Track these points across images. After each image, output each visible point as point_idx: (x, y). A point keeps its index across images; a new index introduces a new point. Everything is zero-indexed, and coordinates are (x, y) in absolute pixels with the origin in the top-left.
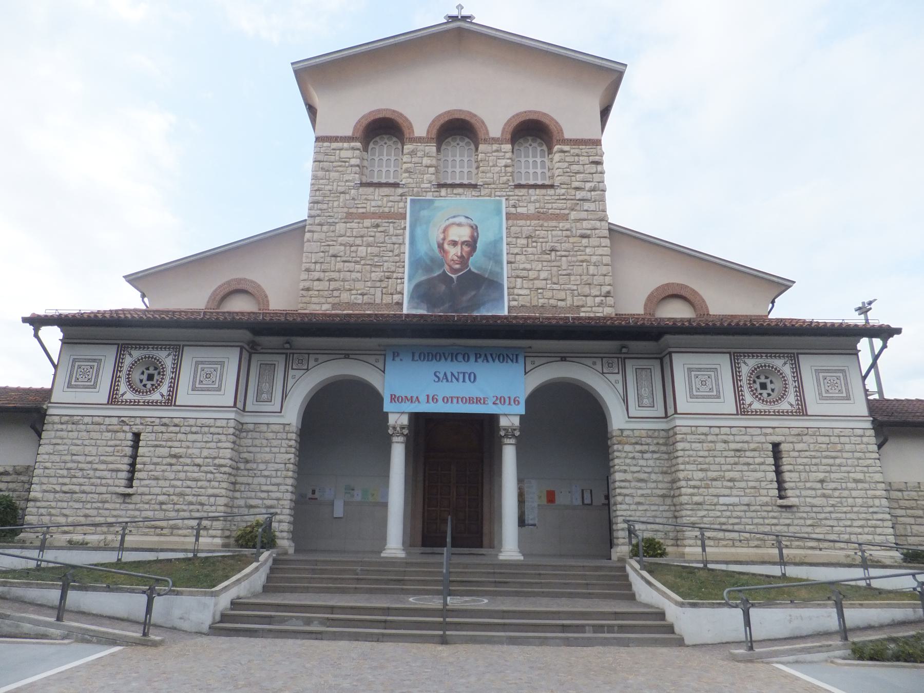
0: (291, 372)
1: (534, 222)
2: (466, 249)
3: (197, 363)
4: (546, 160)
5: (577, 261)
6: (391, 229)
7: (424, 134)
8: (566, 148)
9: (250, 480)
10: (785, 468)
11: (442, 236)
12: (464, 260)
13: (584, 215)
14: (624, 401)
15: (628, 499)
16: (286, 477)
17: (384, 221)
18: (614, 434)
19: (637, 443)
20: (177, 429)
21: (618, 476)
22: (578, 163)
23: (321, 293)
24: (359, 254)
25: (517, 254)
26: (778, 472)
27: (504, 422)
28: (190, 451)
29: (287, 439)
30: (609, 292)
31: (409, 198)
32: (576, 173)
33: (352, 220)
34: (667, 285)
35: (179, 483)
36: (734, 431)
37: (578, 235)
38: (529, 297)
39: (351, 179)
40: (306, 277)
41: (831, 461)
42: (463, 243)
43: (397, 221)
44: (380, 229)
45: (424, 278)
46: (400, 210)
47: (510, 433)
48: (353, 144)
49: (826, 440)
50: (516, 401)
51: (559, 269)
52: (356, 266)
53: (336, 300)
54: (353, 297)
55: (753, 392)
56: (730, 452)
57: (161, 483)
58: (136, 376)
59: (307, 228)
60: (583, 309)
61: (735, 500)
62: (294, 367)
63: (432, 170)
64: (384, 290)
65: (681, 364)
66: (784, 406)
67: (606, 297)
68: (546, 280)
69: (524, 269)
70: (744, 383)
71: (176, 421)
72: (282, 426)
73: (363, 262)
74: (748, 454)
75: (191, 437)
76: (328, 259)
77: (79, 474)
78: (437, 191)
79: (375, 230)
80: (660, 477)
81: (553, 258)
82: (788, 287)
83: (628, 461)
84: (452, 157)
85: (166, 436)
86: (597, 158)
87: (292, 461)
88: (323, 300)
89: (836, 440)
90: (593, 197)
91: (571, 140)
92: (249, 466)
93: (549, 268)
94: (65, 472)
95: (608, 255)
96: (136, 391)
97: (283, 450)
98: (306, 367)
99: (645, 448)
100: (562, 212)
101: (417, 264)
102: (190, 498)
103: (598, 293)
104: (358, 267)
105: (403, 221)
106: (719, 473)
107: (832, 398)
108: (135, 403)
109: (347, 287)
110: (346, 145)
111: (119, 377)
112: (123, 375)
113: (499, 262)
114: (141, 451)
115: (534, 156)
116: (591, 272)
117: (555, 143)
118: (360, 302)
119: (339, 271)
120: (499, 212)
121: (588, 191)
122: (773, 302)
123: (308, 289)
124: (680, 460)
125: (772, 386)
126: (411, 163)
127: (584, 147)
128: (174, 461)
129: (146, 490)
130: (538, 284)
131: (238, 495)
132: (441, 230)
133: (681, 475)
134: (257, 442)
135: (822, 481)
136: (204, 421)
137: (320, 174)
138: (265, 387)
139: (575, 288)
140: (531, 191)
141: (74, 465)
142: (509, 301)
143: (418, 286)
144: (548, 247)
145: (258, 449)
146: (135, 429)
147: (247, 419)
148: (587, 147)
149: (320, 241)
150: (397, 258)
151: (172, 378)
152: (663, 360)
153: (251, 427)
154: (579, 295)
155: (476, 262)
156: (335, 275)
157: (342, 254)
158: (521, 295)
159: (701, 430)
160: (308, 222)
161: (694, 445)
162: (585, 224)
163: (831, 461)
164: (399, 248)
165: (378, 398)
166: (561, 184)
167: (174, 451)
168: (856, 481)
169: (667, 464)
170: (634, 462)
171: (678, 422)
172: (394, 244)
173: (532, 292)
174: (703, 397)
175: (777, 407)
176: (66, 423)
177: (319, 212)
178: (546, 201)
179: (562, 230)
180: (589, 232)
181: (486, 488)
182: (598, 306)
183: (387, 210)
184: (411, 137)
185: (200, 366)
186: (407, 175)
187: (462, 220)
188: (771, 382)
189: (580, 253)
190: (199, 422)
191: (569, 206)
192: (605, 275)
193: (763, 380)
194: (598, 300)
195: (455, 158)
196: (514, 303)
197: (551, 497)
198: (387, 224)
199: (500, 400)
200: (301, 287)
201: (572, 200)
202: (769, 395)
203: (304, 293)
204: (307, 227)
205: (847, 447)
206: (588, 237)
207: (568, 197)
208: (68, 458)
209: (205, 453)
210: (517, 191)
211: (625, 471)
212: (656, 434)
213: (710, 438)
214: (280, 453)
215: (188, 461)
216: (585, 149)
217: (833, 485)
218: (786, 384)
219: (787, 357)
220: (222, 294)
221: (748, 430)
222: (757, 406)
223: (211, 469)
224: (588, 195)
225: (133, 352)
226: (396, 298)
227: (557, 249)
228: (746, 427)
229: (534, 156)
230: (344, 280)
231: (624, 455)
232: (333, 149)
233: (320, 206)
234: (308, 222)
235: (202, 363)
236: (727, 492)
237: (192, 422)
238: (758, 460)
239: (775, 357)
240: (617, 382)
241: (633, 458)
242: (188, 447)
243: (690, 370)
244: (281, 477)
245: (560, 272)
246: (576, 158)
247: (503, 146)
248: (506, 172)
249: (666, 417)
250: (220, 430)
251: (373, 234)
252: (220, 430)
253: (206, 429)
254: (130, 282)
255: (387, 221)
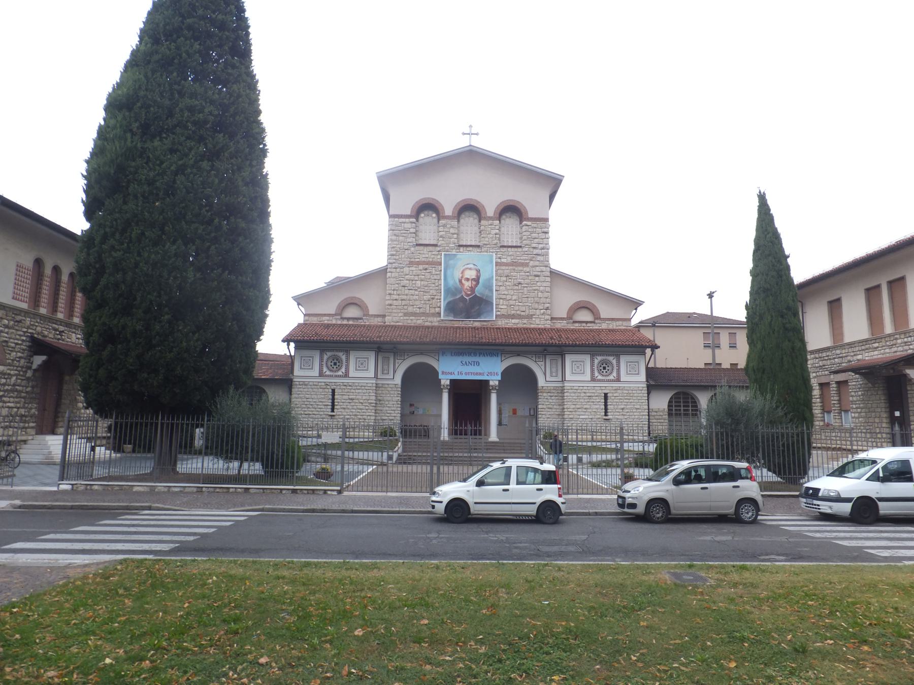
0: (397, 361)
1: (511, 268)
2: (474, 283)
6: (434, 271)
9: (382, 408)
10: (608, 404)
11: (461, 275)
12: (472, 289)
13: (537, 263)
15: (544, 416)
16: (397, 407)
21: (540, 406)
22: (535, 232)
23: (398, 307)
26: (606, 405)
27: (491, 383)
28: (358, 397)
30: (548, 307)
31: (443, 253)
34: (580, 301)
35: (354, 410)
42: (472, 279)
44: (428, 271)
45: (452, 299)
47: (494, 388)
49: (627, 392)
50: (497, 374)
53: (406, 311)
57: (347, 410)
58: (329, 364)
60: (534, 316)
61: (587, 417)
63: (455, 236)
65: (569, 359)
66: (611, 377)
69: (504, 294)
70: (595, 367)
71: (350, 384)
73: (419, 290)
74: (594, 398)
75: (357, 391)
76: (401, 288)
77: (311, 407)
80: (558, 407)
81: (520, 288)
82: (641, 305)
85: (346, 390)
86: (545, 230)
88: (399, 311)
89: (630, 392)
92: (381, 402)
94: (304, 406)
96: (331, 371)
101: (448, 291)
102: (359, 417)
105: (440, 267)
108: (331, 376)
109: (411, 304)
110: (407, 220)
112: (324, 363)
113: (491, 290)
114: (336, 397)
120: (492, 262)
122: (636, 309)
123: (391, 305)
124: (565, 400)
128: (351, 401)
129: (340, 413)
130: (511, 302)
131: (377, 415)
132: (460, 272)
133: (565, 407)
134: (384, 392)
135: (623, 409)
137: (394, 238)
138: (386, 367)
139: (530, 305)
141: (308, 403)
142: (496, 312)
143: (449, 303)
146: (332, 387)
147: (379, 382)
153: (380, 385)
154: (532, 309)
155: (479, 290)
157: (407, 285)
160: (388, 267)
161: (572, 394)
162: (538, 269)
163: (628, 401)
165: (436, 373)
167: (351, 397)
168: (637, 409)
169: (561, 401)
171: (566, 385)
175: (608, 378)
176: (302, 385)
180: (539, 273)
181: (483, 412)
183: (431, 260)
186: (441, 239)
187: (471, 266)
190: (360, 384)
193: (604, 365)
194: (542, 311)
196: (499, 313)
197: (515, 412)
199: (490, 374)
200: (387, 304)
203: (388, 307)
205: (635, 395)
208: (305, 400)
209: (364, 398)
210: (503, 250)
211: (543, 404)
213: (578, 391)
215: (357, 401)
216: (540, 224)
217: (627, 410)
220: (343, 305)
222: (600, 377)
223: (367, 404)
224: (539, 252)
225: (327, 353)
226: (437, 310)
230: (409, 300)
233: (394, 257)
234: (388, 267)
236: (584, 413)
237: (357, 384)
240: (542, 365)
243: (573, 362)
247: (494, 222)
248: (496, 238)
249: (562, 381)
250: (369, 388)
251: (424, 274)
252: (369, 388)
253: (363, 388)
254: (294, 300)
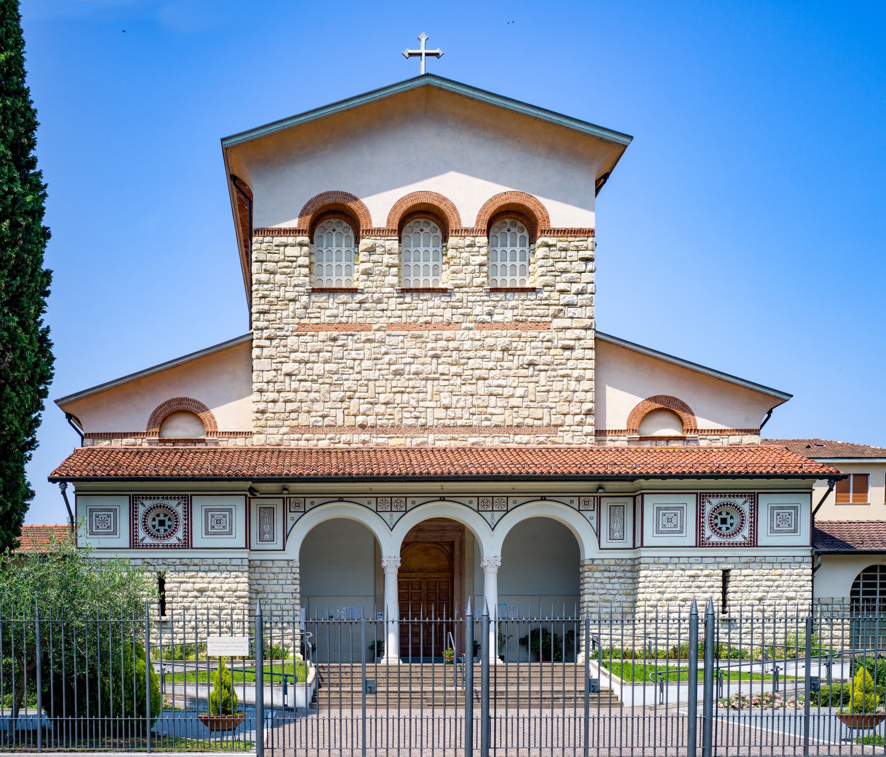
0: (290, 515)
3: (207, 511)
4: (526, 249)
5: (557, 376)
7: (383, 225)
8: (551, 241)
13: (567, 323)
14: (597, 535)
17: (342, 333)
18: (586, 563)
19: (605, 571)
20: (197, 568)
21: (587, 598)
24: (315, 372)
25: (492, 369)
26: (724, 593)
29: (292, 572)
30: (590, 410)
32: (561, 272)
33: (304, 333)
36: (691, 560)
37: (559, 346)
38: (503, 416)
39: (300, 283)
40: (258, 398)
41: (771, 583)
43: (357, 333)
46: (359, 320)
48: (299, 239)
51: (537, 385)
52: (313, 385)
53: (295, 423)
54: (313, 420)
55: (713, 527)
56: (685, 578)
59: (255, 343)
62: (292, 510)
63: (394, 270)
64: (346, 412)
65: (650, 504)
67: (586, 415)
68: (522, 397)
69: (499, 386)
70: (706, 520)
71: (196, 561)
72: (286, 562)
73: (320, 381)
78: (401, 297)
79: (332, 343)
80: (624, 598)
83: (596, 585)
84: (414, 246)
87: (298, 591)
90: (579, 302)
91: (558, 231)
93: (526, 385)
95: (591, 369)
96: (154, 536)
97: (289, 582)
98: (303, 510)
99: (613, 574)
100: (543, 319)
103: (578, 411)
104: (316, 386)
106: (674, 595)
107: (781, 531)
110: (291, 240)
111: (136, 524)
115: (513, 245)
116: (572, 388)
117: (539, 234)
118: (320, 424)
119: (296, 391)
121: (575, 294)
122: (770, 412)
123: (263, 412)
124: (641, 585)
125: (732, 521)
126: (369, 261)
127: (573, 239)
130: (514, 402)
135: (760, 600)
136: (220, 561)
138: (267, 528)
139: (553, 405)
140: (509, 295)
144: (526, 359)
145: (266, 582)
147: (255, 556)
148: (577, 239)
149: (271, 357)
150: (358, 375)
151: (185, 524)
152: (636, 498)
153: (258, 563)
156: (291, 396)
158: (495, 414)
159: (662, 560)
162: (569, 334)
163: (771, 583)
164: (360, 364)
166: (544, 286)
170: (602, 586)
172: (354, 360)
173: (506, 411)
174: (668, 532)
177: (266, 324)
178: (525, 307)
179: (542, 341)
180: (572, 343)
182: (577, 425)
183: (344, 320)
184: (369, 228)
185: (210, 513)
188: (732, 517)
189: (561, 367)
190: (216, 562)
191: (551, 312)
192: (587, 392)
194: (578, 418)
195: (418, 249)
198: (345, 337)
201: (555, 305)
202: (728, 529)
203: (259, 415)
204: (254, 341)
206: (571, 348)
207: (552, 302)
209: (226, 586)
210: (494, 297)
211: (593, 594)
212: (624, 562)
214: (286, 584)
218: (743, 520)
219: (748, 496)
221: (704, 559)
222: (715, 539)
223: (233, 599)
227: (536, 363)
228: (702, 557)
229: (513, 245)
231: (593, 580)
232: (276, 246)
233: (267, 316)
235: (211, 510)
237: (210, 562)
238: (708, 584)
239: (737, 496)
240: (592, 518)
241: (602, 583)
242: (210, 583)
244: (290, 604)
245: (538, 389)
246: (563, 253)
247: (477, 239)
249: (634, 548)
250: (236, 568)
251: (329, 348)
253: (224, 567)
255: (345, 333)
